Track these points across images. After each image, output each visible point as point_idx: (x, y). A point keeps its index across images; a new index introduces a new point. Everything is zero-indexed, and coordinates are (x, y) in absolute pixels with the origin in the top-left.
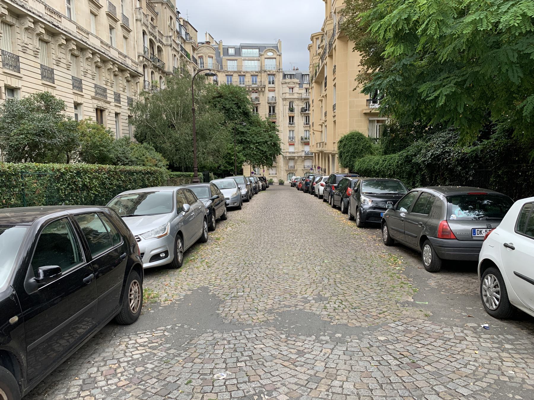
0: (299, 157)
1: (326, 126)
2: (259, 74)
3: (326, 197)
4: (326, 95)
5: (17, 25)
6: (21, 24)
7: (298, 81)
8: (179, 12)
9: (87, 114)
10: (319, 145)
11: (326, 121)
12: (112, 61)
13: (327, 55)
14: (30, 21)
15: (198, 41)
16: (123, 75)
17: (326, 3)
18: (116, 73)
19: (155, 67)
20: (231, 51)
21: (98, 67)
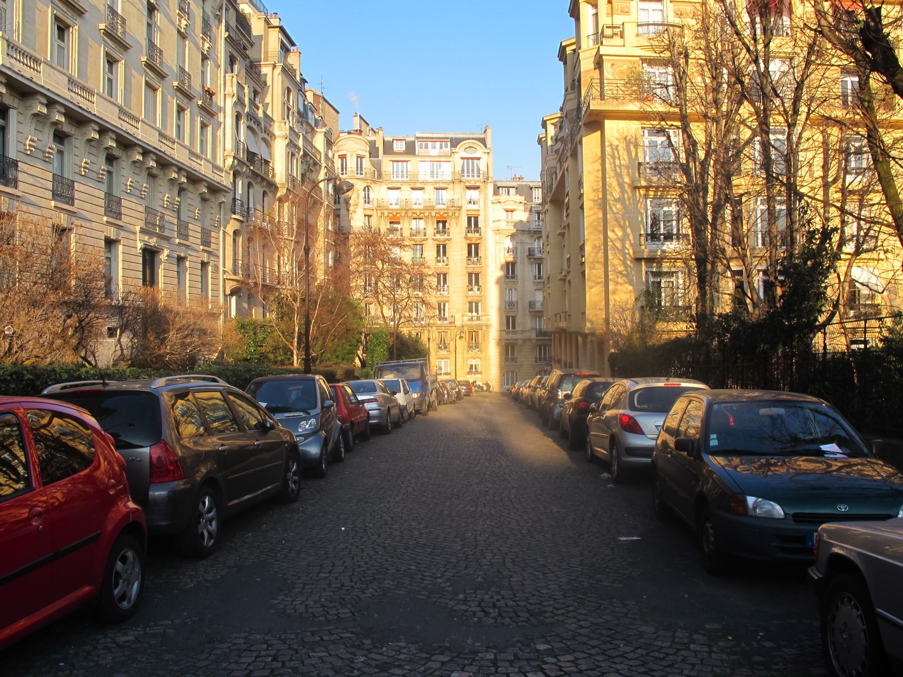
0: (525, 340)
1: (569, 281)
2: (451, 186)
3: (55, 65)
4: (568, 225)
5: (124, 158)
6: (27, 108)
7: (523, 198)
8: (304, 81)
9: (353, 267)
10: (558, 316)
11: (569, 272)
12: (176, 166)
13: (569, 154)
14: (58, 112)
15: (340, 129)
16: (197, 189)
17: (565, 63)
18: (184, 186)
19: (255, 175)
20: (399, 147)
21: (152, 176)
